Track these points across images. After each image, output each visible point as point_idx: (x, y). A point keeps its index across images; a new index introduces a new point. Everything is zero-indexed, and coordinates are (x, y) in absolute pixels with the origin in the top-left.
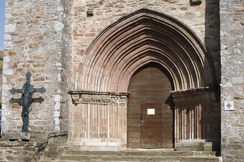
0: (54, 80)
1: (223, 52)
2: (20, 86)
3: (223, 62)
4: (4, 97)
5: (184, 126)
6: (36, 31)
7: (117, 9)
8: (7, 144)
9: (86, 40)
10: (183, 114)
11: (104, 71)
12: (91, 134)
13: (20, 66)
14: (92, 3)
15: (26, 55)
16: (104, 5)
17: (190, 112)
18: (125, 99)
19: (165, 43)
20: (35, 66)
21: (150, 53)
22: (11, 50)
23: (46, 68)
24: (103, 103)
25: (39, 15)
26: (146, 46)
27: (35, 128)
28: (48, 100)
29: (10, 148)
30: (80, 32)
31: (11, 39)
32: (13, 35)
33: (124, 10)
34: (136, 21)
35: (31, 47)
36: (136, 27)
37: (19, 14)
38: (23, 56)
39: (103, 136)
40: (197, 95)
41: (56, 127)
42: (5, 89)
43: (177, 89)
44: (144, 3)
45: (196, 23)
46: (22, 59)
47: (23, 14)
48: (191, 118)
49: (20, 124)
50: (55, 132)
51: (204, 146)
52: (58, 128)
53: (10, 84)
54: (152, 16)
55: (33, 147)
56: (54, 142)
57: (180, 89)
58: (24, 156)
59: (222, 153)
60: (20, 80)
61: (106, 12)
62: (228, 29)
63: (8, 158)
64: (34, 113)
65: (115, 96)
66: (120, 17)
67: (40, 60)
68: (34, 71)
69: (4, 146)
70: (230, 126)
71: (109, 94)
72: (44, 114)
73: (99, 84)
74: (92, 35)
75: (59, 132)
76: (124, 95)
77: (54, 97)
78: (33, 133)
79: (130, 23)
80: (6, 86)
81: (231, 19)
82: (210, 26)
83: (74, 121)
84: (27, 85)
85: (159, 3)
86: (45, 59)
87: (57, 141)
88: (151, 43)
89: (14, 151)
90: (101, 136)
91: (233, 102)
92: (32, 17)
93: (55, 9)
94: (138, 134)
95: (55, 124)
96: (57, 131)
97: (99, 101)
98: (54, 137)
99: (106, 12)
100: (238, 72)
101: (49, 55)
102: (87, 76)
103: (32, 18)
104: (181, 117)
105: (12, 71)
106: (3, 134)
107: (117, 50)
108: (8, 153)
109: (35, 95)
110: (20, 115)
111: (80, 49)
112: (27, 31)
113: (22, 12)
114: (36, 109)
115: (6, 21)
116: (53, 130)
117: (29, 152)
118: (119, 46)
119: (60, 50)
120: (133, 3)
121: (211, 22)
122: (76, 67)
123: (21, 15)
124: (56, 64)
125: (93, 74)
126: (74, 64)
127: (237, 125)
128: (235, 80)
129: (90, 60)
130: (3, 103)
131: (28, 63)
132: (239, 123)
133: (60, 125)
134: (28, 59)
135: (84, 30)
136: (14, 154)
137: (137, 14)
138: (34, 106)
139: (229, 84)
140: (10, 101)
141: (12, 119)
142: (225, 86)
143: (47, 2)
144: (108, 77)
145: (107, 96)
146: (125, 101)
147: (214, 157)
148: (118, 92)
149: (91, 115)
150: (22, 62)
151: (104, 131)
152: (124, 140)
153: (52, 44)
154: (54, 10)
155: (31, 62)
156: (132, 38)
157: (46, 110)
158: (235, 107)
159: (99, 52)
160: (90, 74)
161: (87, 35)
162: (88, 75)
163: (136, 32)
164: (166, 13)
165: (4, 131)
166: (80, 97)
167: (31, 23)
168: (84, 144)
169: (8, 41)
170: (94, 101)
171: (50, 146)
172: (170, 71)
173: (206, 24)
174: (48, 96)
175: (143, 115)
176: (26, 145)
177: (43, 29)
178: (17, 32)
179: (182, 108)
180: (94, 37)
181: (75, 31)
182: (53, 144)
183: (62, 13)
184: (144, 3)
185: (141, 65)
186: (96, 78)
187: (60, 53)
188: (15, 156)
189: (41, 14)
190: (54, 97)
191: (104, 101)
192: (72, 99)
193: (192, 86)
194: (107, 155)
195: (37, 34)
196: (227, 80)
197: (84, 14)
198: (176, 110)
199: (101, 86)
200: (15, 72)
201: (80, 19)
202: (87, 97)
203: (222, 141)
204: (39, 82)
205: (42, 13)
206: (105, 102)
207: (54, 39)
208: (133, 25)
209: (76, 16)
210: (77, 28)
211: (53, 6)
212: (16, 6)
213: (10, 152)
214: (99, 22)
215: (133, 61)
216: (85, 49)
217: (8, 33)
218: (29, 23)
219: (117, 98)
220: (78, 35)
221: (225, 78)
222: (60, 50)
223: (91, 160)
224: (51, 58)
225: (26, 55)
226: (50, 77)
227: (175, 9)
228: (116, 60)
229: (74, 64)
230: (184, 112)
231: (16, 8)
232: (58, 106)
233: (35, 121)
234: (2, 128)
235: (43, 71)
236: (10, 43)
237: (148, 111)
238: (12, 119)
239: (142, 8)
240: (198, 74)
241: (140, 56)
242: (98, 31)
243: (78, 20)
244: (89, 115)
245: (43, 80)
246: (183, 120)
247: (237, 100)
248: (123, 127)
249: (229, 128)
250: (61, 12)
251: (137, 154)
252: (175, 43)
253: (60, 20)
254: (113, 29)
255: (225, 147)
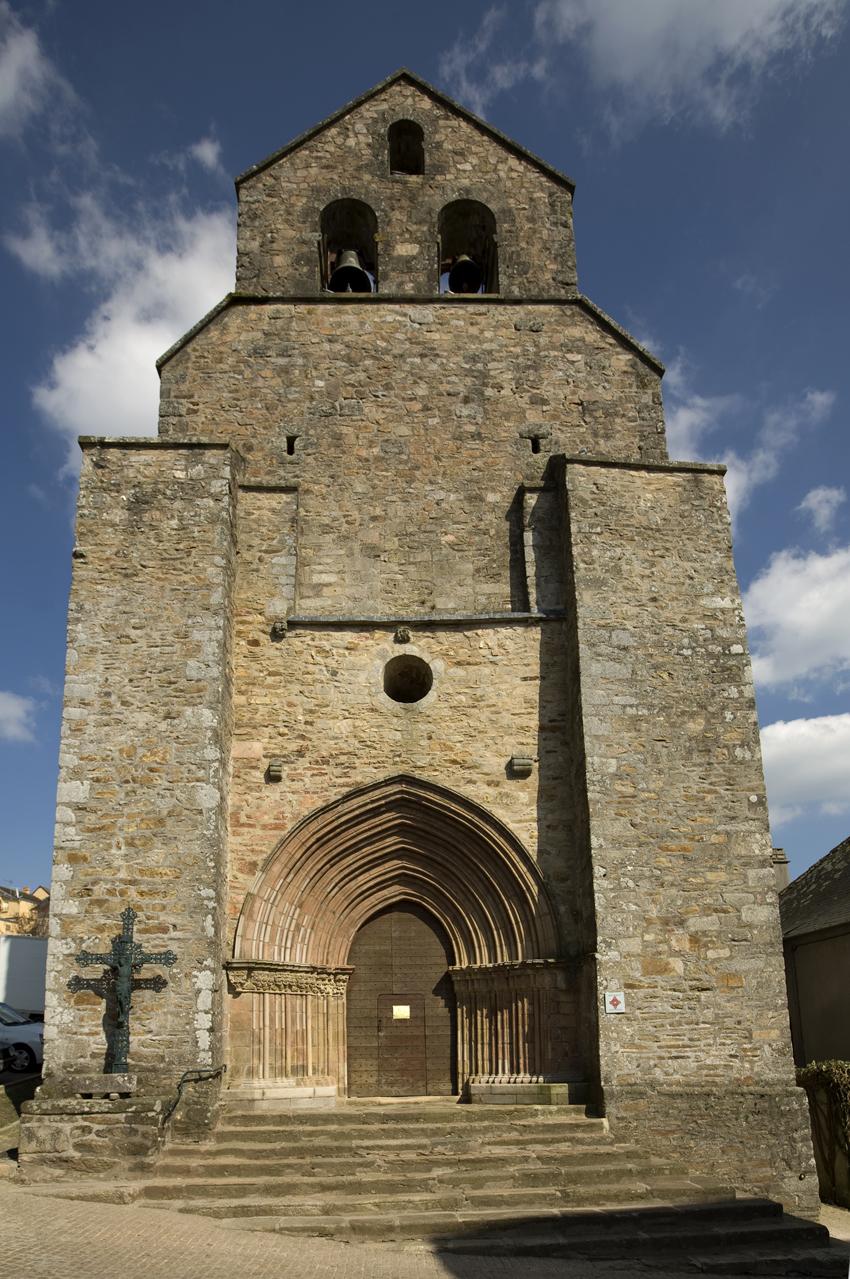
0: (194, 933)
1: (599, 884)
2: (103, 945)
3: (600, 904)
4: (54, 973)
5: (483, 1044)
6: (145, 805)
7: (339, 771)
8: (78, 1107)
9: (262, 839)
10: (479, 1018)
11: (300, 915)
12: (272, 1068)
13: (99, 891)
14: (277, 752)
15: (116, 864)
16: (307, 759)
17: (499, 1014)
18: (344, 982)
19: (443, 858)
20: (142, 894)
21: (402, 879)
22: (73, 849)
23: (173, 899)
24: (299, 993)
25: (155, 765)
26: (396, 862)
27: (141, 1057)
28: (178, 983)
29: (85, 1120)
30: (248, 817)
31: (74, 820)
32: (80, 809)
33: (357, 775)
34: (383, 802)
35: (131, 844)
36: (381, 817)
37: (98, 757)
38: (109, 866)
39: (300, 1070)
40: (519, 976)
41: (202, 1055)
42: (55, 951)
43: (463, 963)
44: (402, 762)
45: (520, 818)
46: (107, 874)
47: (109, 758)
48: (503, 1028)
49: (99, 1046)
50: (199, 1068)
51: (552, 1092)
52: (205, 1058)
53: (69, 940)
54: (422, 793)
55: (153, 1114)
56: (197, 1095)
57: (490, 962)
58: (126, 1141)
59: (608, 1110)
60: (101, 929)
61: (313, 775)
62: (606, 832)
63: (78, 1146)
64: (138, 1019)
65: (325, 976)
66: (347, 789)
67: (157, 879)
68: (140, 908)
69: (68, 1114)
70: (618, 1048)
71: (313, 969)
72: (166, 1020)
73: (289, 945)
74: (277, 827)
75: (208, 1068)
76: (344, 974)
77: (196, 977)
78: (137, 1070)
79: (371, 806)
80: (59, 943)
81: (612, 812)
82: (548, 827)
83: (232, 1036)
84: (121, 943)
85: (439, 765)
86: (171, 878)
87: (206, 1093)
88: (408, 856)
89: (96, 1127)
90: (295, 1071)
91: (622, 993)
92: (136, 767)
93: (198, 753)
94: (370, 1065)
95: (197, 1046)
96: (205, 1066)
97: (290, 986)
98: (196, 1081)
99: (313, 775)
100: (631, 929)
101: (181, 866)
102: (264, 926)
103: (136, 771)
104: (473, 1025)
105: (77, 903)
106: (49, 1075)
107: (332, 866)
108: (79, 1132)
109: (146, 972)
110: (101, 1022)
111: (248, 859)
112: (121, 802)
113: (109, 753)
114: (146, 1008)
115: (63, 773)
116: (193, 1062)
117: (141, 1128)
118: (337, 859)
119: (212, 856)
120: (379, 759)
121: (550, 816)
122: (238, 903)
123: (104, 760)
124: (200, 890)
125: (277, 923)
126: (233, 895)
127: (632, 1045)
128: (626, 945)
129: (273, 889)
130: (50, 990)
131: (123, 887)
132: (636, 1041)
133: (211, 1049)
134: (122, 875)
135: (258, 814)
136: (98, 1135)
137: (387, 785)
138: (141, 999)
139: (613, 954)
140: (69, 985)
141: (75, 1033)
142: (606, 958)
143: (177, 734)
144: (309, 931)
145: (309, 975)
146: (343, 988)
147: (583, 1119)
148: (333, 966)
149: (272, 1020)
150: (106, 881)
151: (301, 1059)
152: (344, 1078)
153: (191, 840)
154: (194, 754)
155: (133, 882)
156: (369, 841)
157: (172, 1008)
158: (627, 1005)
159: (294, 869)
160: (270, 922)
161: (264, 827)
162: (267, 924)
163: (379, 829)
164: (455, 789)
165: (52, 1065)
166: (249, 976)
167: (132, 784)
168: (264, 1094)
169: (67, 824)
170: (279, 986)
171: (187, 1104)
172: (446, 922)
173: (539, 820)
174: (179, 973)
175: (383, 1020)
176: (133, 1108)
177: (167, 799)
178: (93, 804)
179: (476, 1004)
180: (285, 833)
181: (235, 815)
182: (195, 1099)
183: (216, 764)
184: (402, 762)
185: (380, 906)
186: (282, 931)
187: (212, 864)
188: (100, 1141)
189: (160, 764)
190: (196, 977)
191: (300, 988)
192: (229, 980)
193: (502, 956)
194: (333, 1124)
195: (148, 813)
196: (609, 945)
197: (259, 776)
198: (459, 1010)
199: (294, 951)
200: (86, 906)
201: (248, 788)
202: (266, 978)
203: (603, 1083)
204: (153, 936)
205: (163, 759)
206: (302, 990)
207: (195, 827)
208: (375, 812)
209: (237, 779)
210: (240, 808)
211: (193, 745)
212: (92, 738)
213: (85, 1130)
214: (295, 797)
215: (364, 895)
216: (260, 859)
217: (68, 805)
218: (127, 782)
219: (330, 980)
220: (243, 825)
221: (604, 941)
222: (212, 856)
223: (300, 1139)
224: (187, 876)
225: (116, 864)
226: (185, 925)
227: (474, 783)
228: (329, 890)
229: (233, 895)
230: (482, 1017)
231: (92, 742)
232: (205, 1000)
233: (143, 1038)
234: (45, 1057)
235: (164, 908)
236: (71, 830)
237: (773, 1029)
238: (75, 1033)
239: (401, 773)
240: (519, 930)
241: (381, 886)
242: (292, 819)
243: (242, 788)
244: (267, 1023)
245: (165, 930)
246: (479, 1031)
247: (630, 991)
248: (341, 1047)
249: (617, 1052)
250: (214, 761)
251: (407, 1120)
252: (466, 860)
253: (211, 780)
254: (329, 816)
255: (612, 1095)
